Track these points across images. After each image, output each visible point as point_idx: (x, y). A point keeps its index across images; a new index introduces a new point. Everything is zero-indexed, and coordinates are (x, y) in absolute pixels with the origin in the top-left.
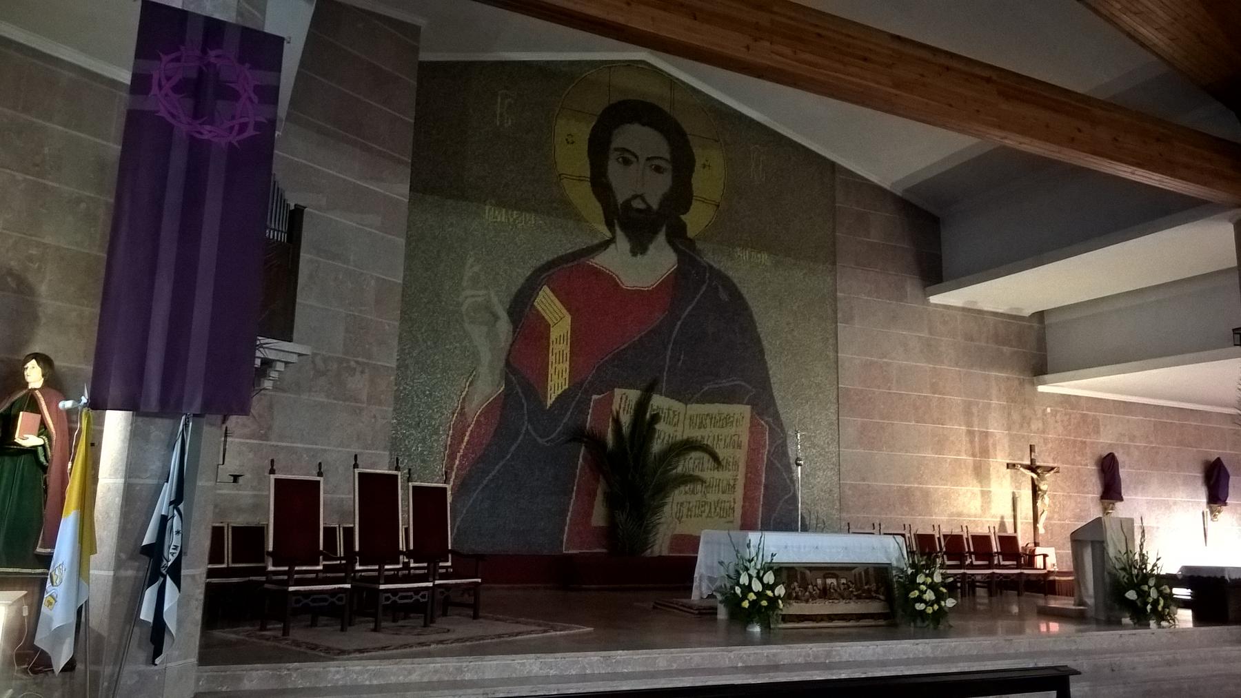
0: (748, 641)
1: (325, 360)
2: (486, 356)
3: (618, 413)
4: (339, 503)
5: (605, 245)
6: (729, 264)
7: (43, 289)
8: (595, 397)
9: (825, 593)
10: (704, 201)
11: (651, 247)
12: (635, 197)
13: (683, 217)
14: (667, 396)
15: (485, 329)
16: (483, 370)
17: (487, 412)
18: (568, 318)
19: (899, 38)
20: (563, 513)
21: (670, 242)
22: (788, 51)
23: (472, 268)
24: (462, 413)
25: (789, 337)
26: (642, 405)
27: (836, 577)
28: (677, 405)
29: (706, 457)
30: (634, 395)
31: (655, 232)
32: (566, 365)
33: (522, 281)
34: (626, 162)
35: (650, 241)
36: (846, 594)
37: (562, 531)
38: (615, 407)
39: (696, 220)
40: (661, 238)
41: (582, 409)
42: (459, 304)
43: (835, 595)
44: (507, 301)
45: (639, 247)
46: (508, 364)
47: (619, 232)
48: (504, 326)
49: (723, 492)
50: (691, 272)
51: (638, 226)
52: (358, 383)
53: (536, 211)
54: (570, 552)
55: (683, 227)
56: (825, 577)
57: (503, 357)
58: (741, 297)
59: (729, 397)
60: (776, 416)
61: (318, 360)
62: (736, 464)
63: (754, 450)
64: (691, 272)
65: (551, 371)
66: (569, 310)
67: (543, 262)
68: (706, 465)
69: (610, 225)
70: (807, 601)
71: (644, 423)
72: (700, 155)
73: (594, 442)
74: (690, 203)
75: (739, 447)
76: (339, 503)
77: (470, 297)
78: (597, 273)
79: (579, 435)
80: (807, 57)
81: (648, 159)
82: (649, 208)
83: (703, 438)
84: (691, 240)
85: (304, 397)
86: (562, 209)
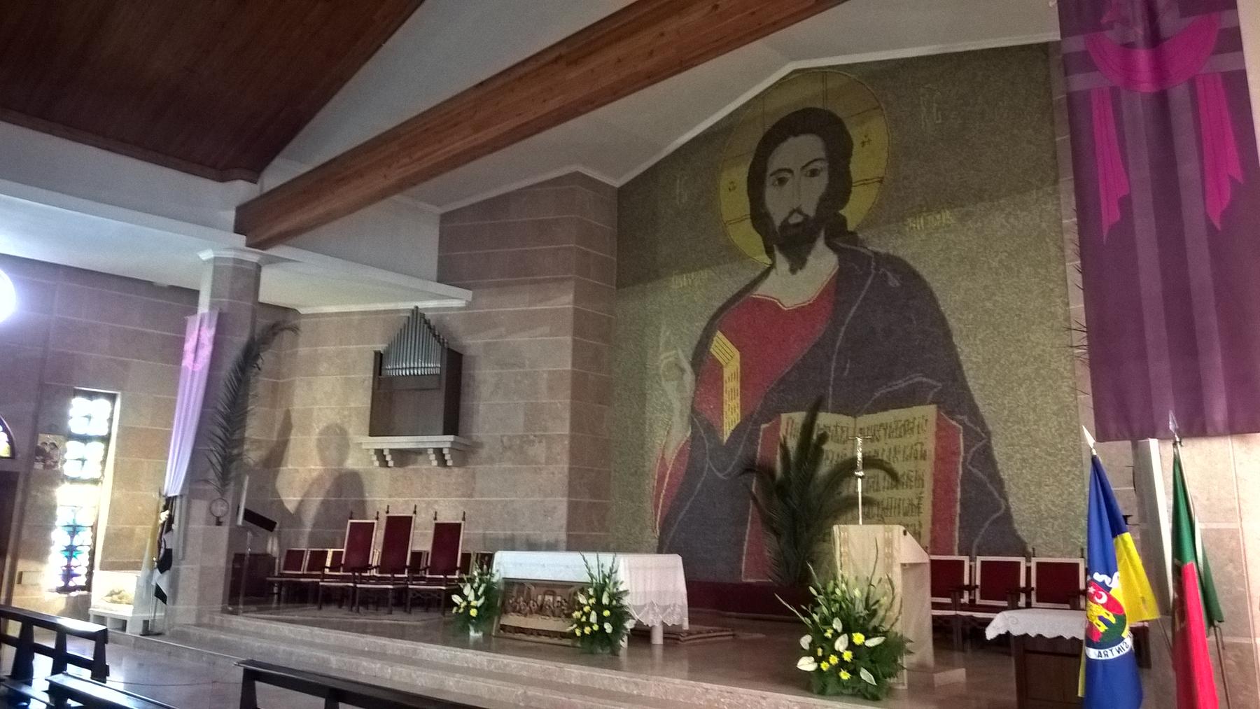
0: (464, 644)
1: (510, 438)
2: (677, 405)
3: (785, 438)
4: (421, 541)
5: (766, 273)
6: (900, 241)
7: (351, 431)
8: (763, 426)
9: (541, 610)
10: (865, 182)
11: (810, 258)
12: (791, 214)
13: (842, 212)
14: (833, 412)
15: (675, 383)
16: (676, 418)
17: (681, 453)
18: (737, 355)
19: (481, 84)
20: (740, 543)
21: (829, 244)
22: (406, 160)
23: (665, 333)
24: (663, 458)
25: (989, 305)
26: (808, 427)
27: (554, 594)
28: (845, 420)
29: (881, 474)
30: (799, 417)
31: (811, 241)
32: (737, 401)
33: (700, 332)
34: (782, 181)
35: (809, 252)
36: (557, 611)
37: (741, 560)
38: (782, 433)
39: (854, 212)
40: (820, 244)
41: (752, 441)
42: (658, 367)
43: (548, 612)
44: (690, 353)
45: (798, 263)
46: (693, 410)
47: (779, 256)
48: (689, 377)
49: (905, 514)
50: (857, 265)
51: (791, 242)
52: (538, 451)
53: (708, 266)
54: (749, 580)
55: (843, 221)
56: (545, 594)
57: (689, 403)
58: (915, 276)
59: (909, 398)
60: (974, 412)
61: (505, 439)
62: (920, 479)
63: (944, 457)
64: (857, 265)
65: (726, 407)
66: (737, 348)
67: (715, 310)
68: (882, 484)
69: (769, 252)
70: (525, 615)
71: (811, 446)
72: (856, 134)
73: (765, 472)
74: (849, 192)
75: (924, 457)
76: (421, 541)
77: (664, 359)
78: (760, 303)
79: (750, 467)
80: (419, 154)
81: (803, 168)
82: (806, 217)
83: (876, 452)
84: (852, 233)
85: (497, 466)
86: (732, 254)
